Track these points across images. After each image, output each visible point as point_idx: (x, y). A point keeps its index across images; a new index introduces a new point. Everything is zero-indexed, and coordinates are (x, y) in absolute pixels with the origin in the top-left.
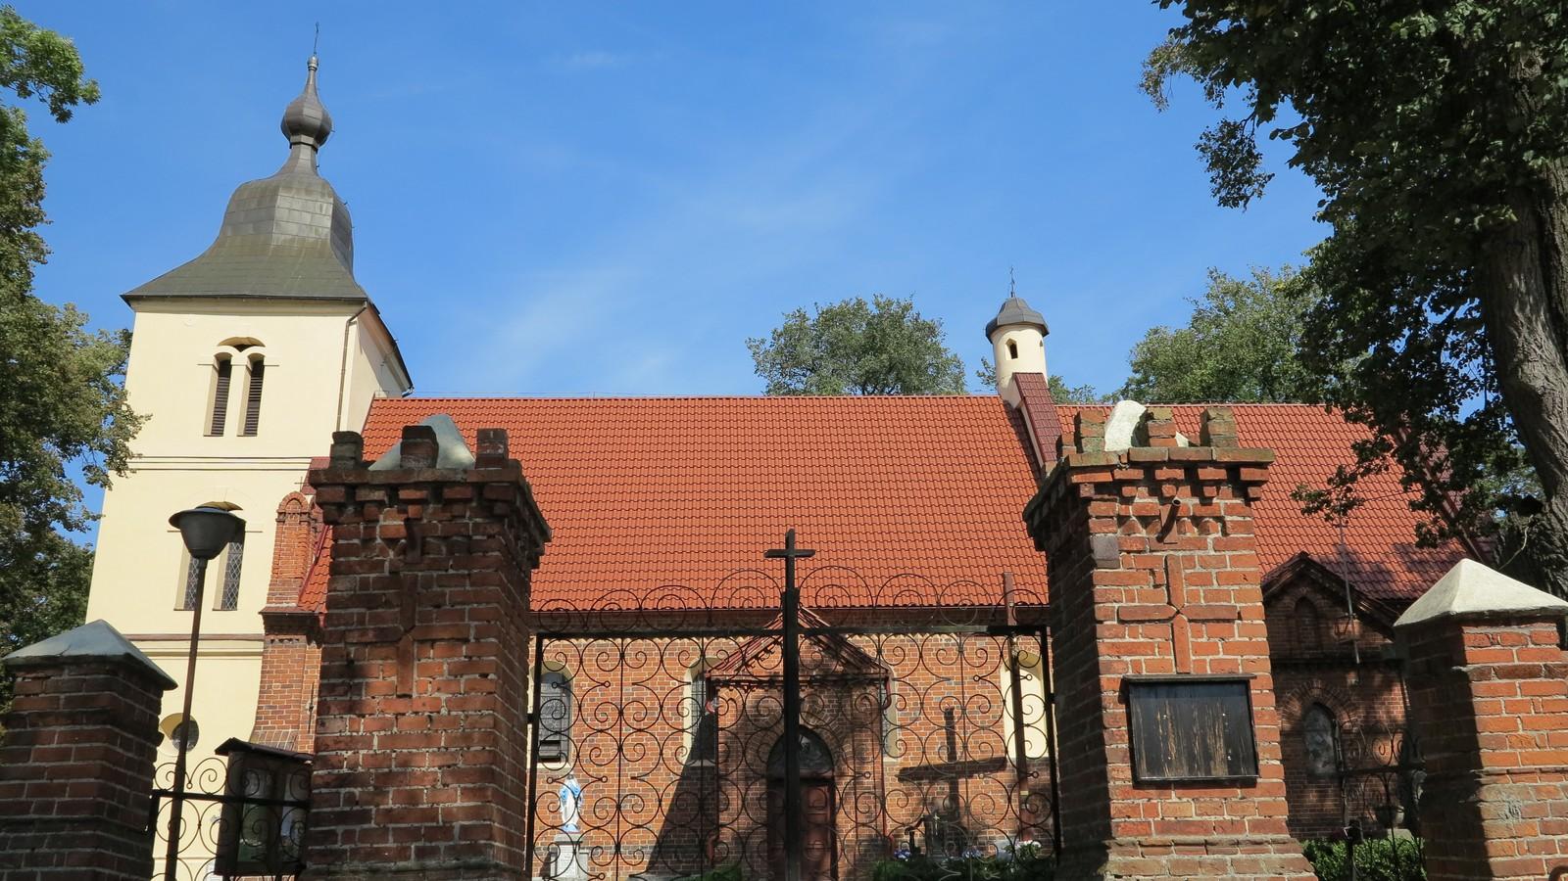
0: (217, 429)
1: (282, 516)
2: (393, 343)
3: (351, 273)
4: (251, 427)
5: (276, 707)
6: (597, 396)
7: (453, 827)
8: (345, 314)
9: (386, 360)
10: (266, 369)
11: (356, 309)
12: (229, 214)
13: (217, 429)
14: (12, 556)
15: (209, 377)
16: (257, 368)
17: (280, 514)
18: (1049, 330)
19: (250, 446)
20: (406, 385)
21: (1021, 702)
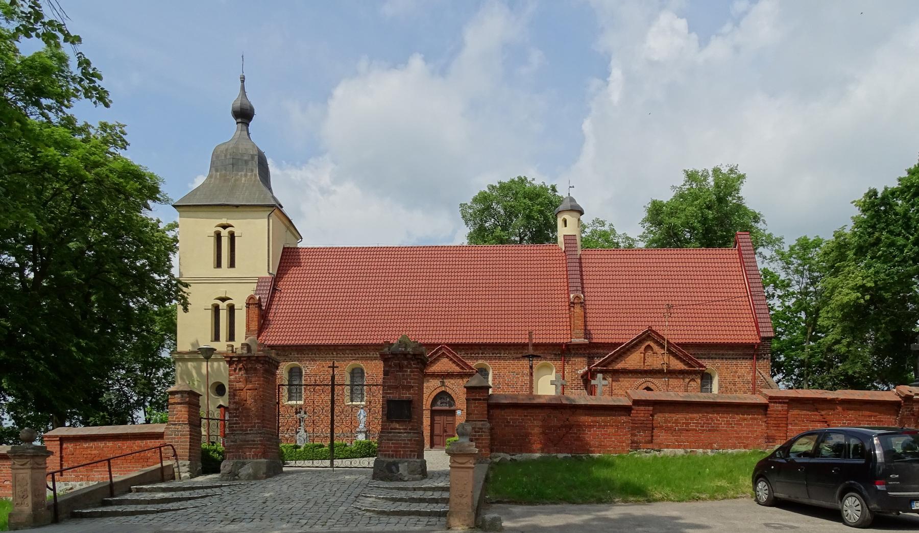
0: (219, 265)
1: (248, 305)
2: (290, 221)
3: (270, 189)
4: (232, 264)
5: (247, 430)
6: (380, 246)
7: (876, 351)
8: (269, 211)
9: (288, 228)
10: (236, 311)
11: (272, 209)
12: (212, 162)
13: (219, 265)
14: (42, 185)
15: (212, 242)
16: (232, 237)
17: (247, 304)
18: (582, 206)
19: (232, 273)
20: (299, 237)
21: (431, 423)
